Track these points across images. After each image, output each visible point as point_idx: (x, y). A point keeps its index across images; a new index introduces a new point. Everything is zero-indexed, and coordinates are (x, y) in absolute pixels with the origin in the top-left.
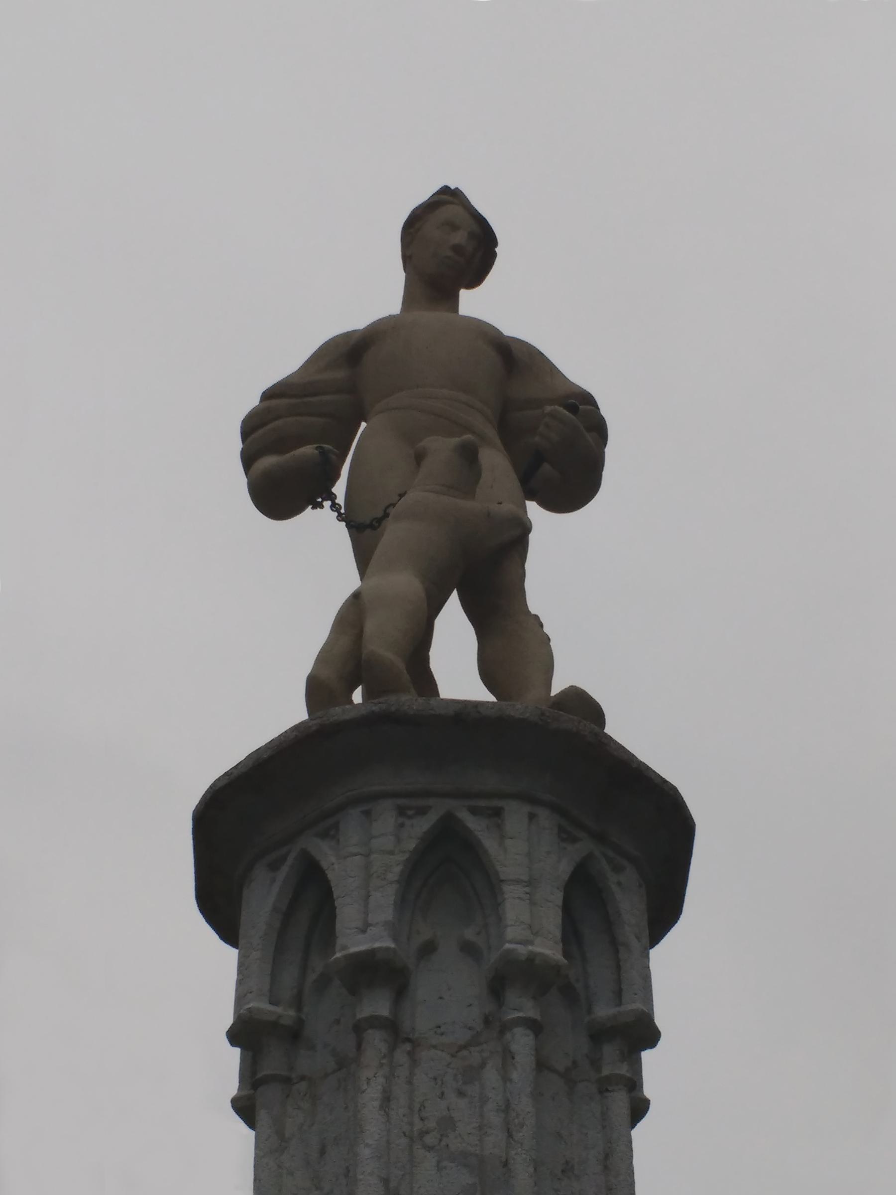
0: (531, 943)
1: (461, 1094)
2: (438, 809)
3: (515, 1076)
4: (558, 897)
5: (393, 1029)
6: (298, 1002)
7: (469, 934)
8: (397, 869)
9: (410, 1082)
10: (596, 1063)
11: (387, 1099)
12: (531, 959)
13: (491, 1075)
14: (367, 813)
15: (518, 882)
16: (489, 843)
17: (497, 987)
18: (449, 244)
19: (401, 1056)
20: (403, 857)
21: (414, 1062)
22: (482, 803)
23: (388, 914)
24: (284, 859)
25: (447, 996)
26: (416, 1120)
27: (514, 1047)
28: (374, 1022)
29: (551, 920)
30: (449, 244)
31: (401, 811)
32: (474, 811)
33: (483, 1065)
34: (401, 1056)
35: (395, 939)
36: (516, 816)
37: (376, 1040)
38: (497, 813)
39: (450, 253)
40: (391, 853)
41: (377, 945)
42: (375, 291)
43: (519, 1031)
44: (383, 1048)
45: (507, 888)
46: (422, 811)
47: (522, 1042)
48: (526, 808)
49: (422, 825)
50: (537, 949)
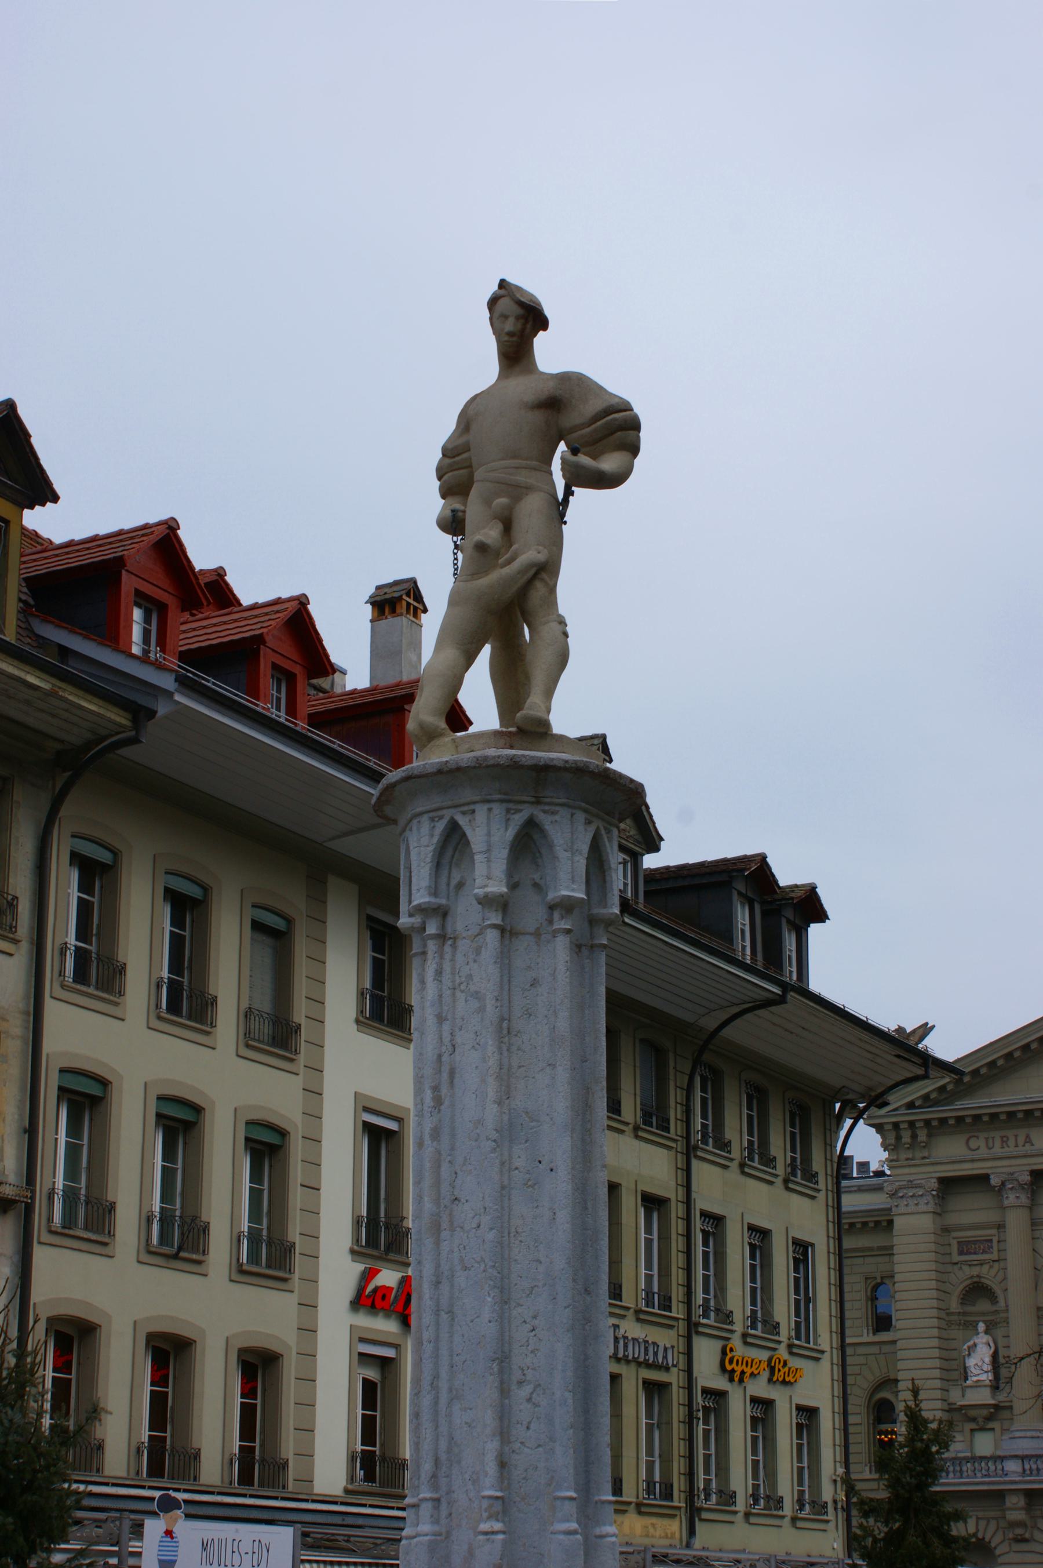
0: (486, 886)
4: (505, 853)
5: (442, 937)
7: (536, 877)
10: (551, 922)
11: (439, 973)
18: (519, 319)
20: (431, 848)
21: (454, 946)
22: (465, 808)
26: (457, 977)
29: (500, 866)
30: (519, 319)
31: (432, 819)
34: (447, 948)
36: (481, 810)
38: (474, 811)
39: (506, 338)
42: (481, 365)
43: (489, 931)
45: (476, 857)
46: (441, 818)
48: (486, 806)
49: (441, 826)
50: (489, 889)
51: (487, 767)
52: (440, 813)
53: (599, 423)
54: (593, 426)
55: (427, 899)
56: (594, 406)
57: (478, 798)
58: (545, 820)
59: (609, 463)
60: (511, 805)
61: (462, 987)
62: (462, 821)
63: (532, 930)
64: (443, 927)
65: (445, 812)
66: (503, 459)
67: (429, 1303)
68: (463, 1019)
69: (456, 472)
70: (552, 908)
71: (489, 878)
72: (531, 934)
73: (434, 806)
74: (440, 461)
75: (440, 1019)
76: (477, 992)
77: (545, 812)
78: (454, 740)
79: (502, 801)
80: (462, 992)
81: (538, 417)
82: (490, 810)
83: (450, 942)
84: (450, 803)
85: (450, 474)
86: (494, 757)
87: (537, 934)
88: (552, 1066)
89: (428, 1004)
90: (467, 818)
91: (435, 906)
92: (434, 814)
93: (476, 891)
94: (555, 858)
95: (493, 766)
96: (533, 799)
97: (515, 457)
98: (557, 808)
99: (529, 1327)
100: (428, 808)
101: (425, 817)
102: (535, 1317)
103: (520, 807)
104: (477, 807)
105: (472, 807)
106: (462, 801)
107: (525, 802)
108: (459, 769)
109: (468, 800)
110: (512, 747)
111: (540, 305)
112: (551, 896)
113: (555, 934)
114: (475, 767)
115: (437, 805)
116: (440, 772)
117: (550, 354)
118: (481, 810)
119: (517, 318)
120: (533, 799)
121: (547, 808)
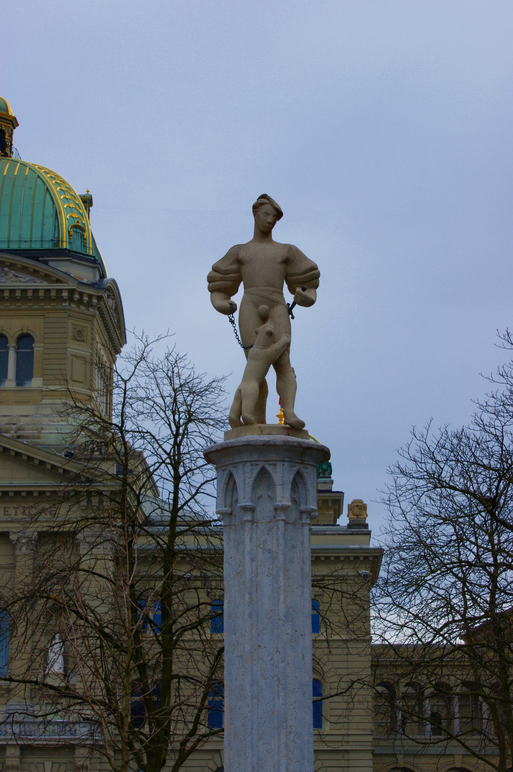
1: (268, 534)
2: (261, 464)
3: (279, 533)
5: (252, 522)
6: (231, 506)
7: (270, 494)
8: (251, 482)
9: (256, 533)
10: (301, 519)
11: (251, 538)
12: (282, 506)
13: (274, 530)
14: (244, 465)
15: (279, 485)
16: (273, 474)
17: (276, 509)
18: (267, 213)
19: (254, 527)
22: (271, 463)
23: (249, 496)
24: (226, 470)
25: (264, 510)
27: (279, 526)
28: (248, 521)
29: (288, 493)
30: (267, 213)
31: (252, 465)
32: (269, 465)
33: (273, 528)
34: (254, 527)
35: (252, 501)
37: (248, 525)
38: (275, 465)
39: (267, 225)
40: (250, 478)
41: (247, 504)
42: (245, 232)
44: (250, 526)
46: (257, 465)
47: (281, 524)
48: (282, 463)
49: (257, 469)
50: (283, 503)
51: (289, 446)
52: (257, 463)
53: (308, 274)
54: (305, 275)
55: (250, 504)
56: (304, 266)
57: (279, 459)
58: (304, 471)
59: (308, 293)
60: (292, 464)
61: (261, 546)
62: (269, 468)
63: (292, 522)
64: (253, 517)
65: (259, 463)
66: (266, 286)
67: (249, 694)
68: (262, 562)
69: (224, 282)
70: (302, 512)
71: (283, 497)
72: (292, 524)
73: (254, 459)
74: (210, 273)
75: (252, 560)
76: (269, 549)
77: (304, 467)
78: (260, 428)
79: (289, 461)
80: (261, 548)
81: (281, 267)
82: (283, 465)
83: (256, 524)
84: (263, 459)
85: (221, 282)
86: (292, 442)
87: (294, 524)
88: (303, 587)
89: (246, 553)
90: (272, 467)
91: (252, 507)
92: (253, 463)
93: (277, 503)
94: (306, 489)
95: (291, 446)
96: (301, 462)
97: (273, 286)
98: (309, 466)
99: (293, 707)
100: (249, 460)
101: (248, 463)
102: (295, 703)
103: (295, 464)
104: (278, 463)
105: (275, 462)
106: (270, 459)
107: (297, 463)
108: (275, 445)
109: (274, 459)
110: (289, 435)
111: (279, 208)
112: (303, 507)
113: (303, 525)
114: (283, 445)
115: (256, 459)
116: (264, 445)
117: (281, 234)
118: (279, 465)
119: (274, 216)
120: (301, 462)
121: (305, 466)
